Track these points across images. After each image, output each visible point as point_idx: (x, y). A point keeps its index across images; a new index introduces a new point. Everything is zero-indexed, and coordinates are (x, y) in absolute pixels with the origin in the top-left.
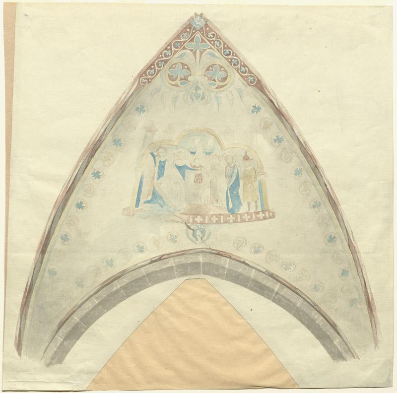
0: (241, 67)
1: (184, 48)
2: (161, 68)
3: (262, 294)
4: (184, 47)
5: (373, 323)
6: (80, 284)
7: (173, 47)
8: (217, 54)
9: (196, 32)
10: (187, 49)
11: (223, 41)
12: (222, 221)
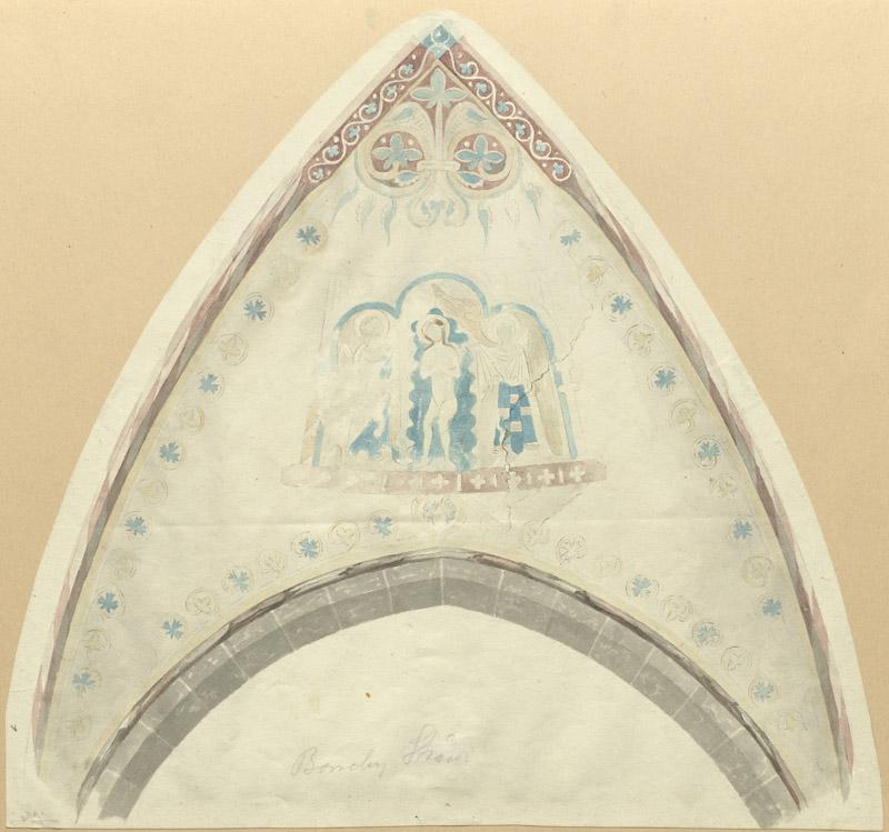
0: (535, 140)
1: (409, 98)
2: (570, 167)
3: (238, 684)
4: (409, 97)
5: (758, 735)
6: (174, 628)
7: (510, 117)
8: (485, 114)
9: (436, 65)
10: (414, 101)
11: (494, 82)
12: (562, 480)
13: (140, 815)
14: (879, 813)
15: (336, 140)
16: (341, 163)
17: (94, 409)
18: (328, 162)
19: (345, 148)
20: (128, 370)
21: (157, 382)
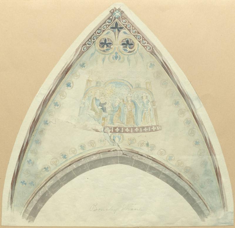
9: (116, 22)
13: (39, 221)
14: (233, 210)
15: (100, 28)
16: (100, 35)
17: (21, 121)
18: (98, 35)
19: (102, 31)
20: (222, 155)
21: (43, 100)
